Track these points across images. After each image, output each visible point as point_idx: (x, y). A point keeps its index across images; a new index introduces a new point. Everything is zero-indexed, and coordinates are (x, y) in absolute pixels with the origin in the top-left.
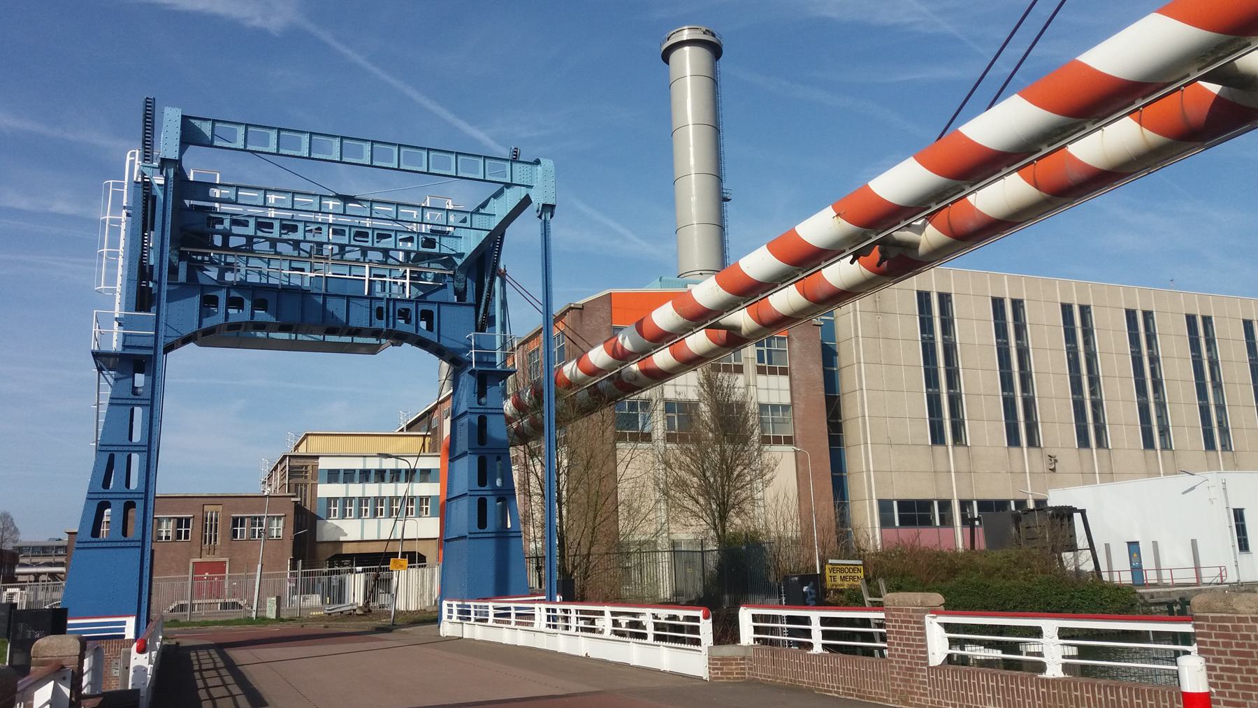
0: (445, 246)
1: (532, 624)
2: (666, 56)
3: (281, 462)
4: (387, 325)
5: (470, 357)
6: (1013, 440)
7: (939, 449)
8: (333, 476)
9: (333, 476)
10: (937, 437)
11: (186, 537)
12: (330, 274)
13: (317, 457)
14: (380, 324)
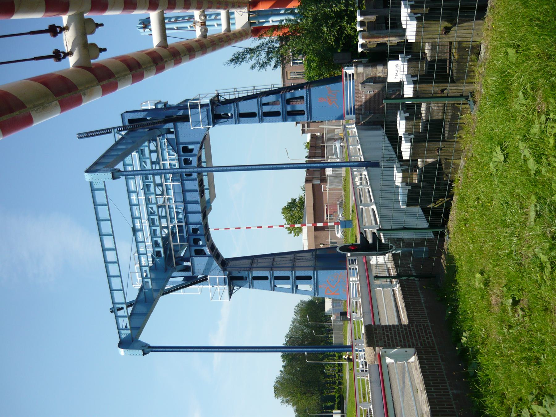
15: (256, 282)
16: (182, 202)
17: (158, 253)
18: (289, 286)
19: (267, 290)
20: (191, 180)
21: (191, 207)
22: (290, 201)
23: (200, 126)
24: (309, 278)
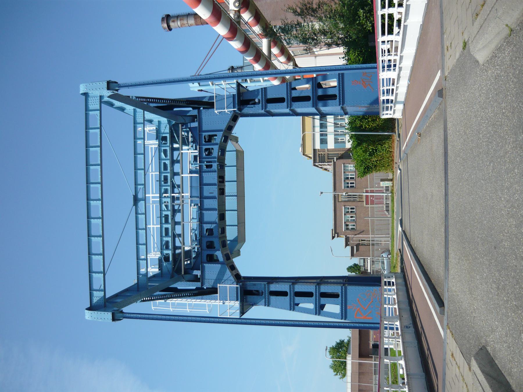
0: (166, 130)
1: (394, 79)
3: (317, 166)
4: (215, 162)
5: (231, 112)
8: (324, 141)
9: (324, 141)
11: (353, 209)
12: (188, 194)
13: (315, 150)
14: (215, 166)
15: (273, 298)
16: (197, 197)
17: (167, 259)
18: (311, 306)
19: (285, 309)
20: (210, 172)
21: (208, 203)
22: (338, 341)
23: (224, 109)
24: (336, 296)
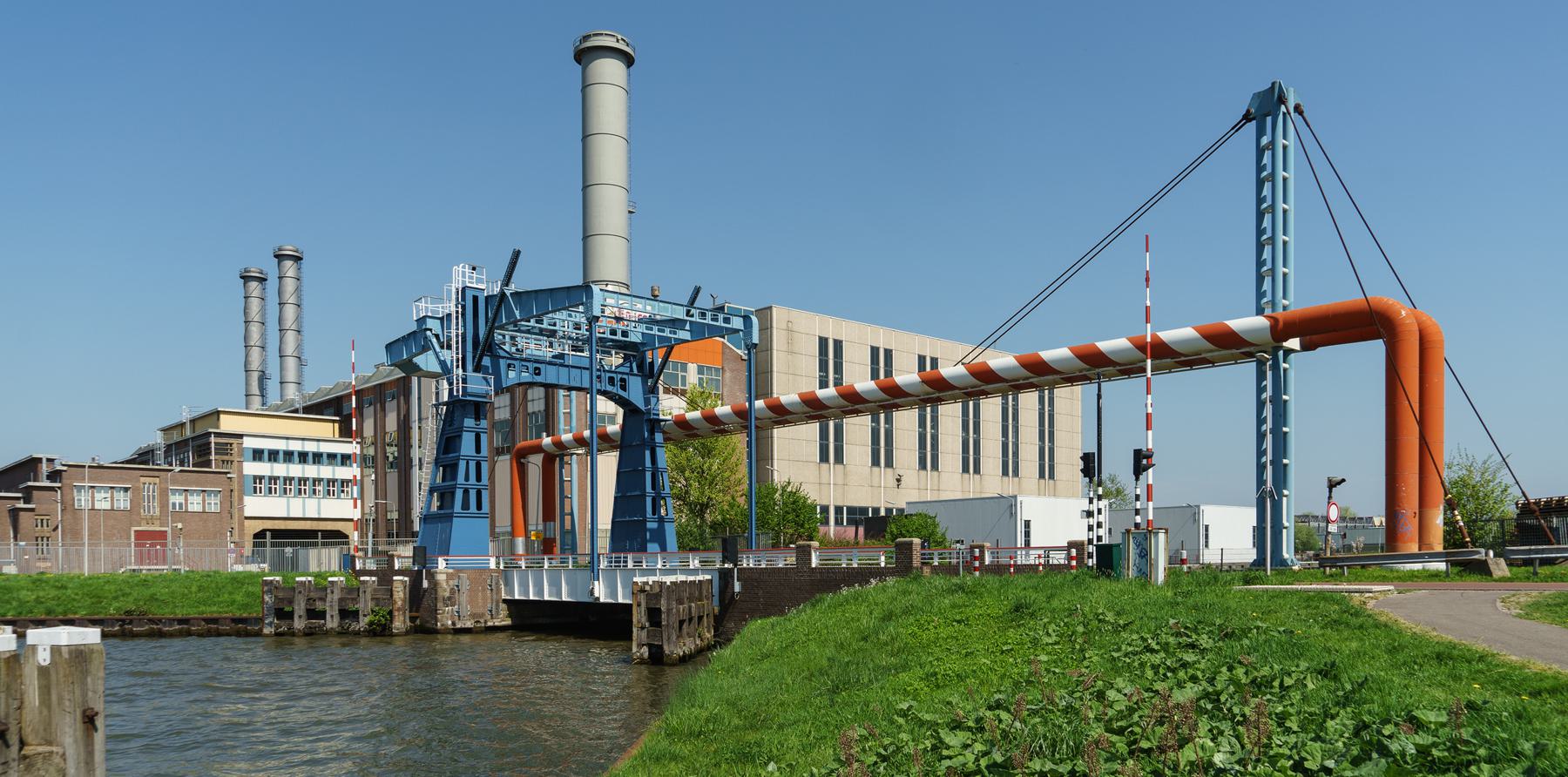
2: (584, 55)
6: (876, 462)
7: (824, 466)
8: (258, 455)
9: (258, 455)
10: (824, 458)
13: (241, 436)
